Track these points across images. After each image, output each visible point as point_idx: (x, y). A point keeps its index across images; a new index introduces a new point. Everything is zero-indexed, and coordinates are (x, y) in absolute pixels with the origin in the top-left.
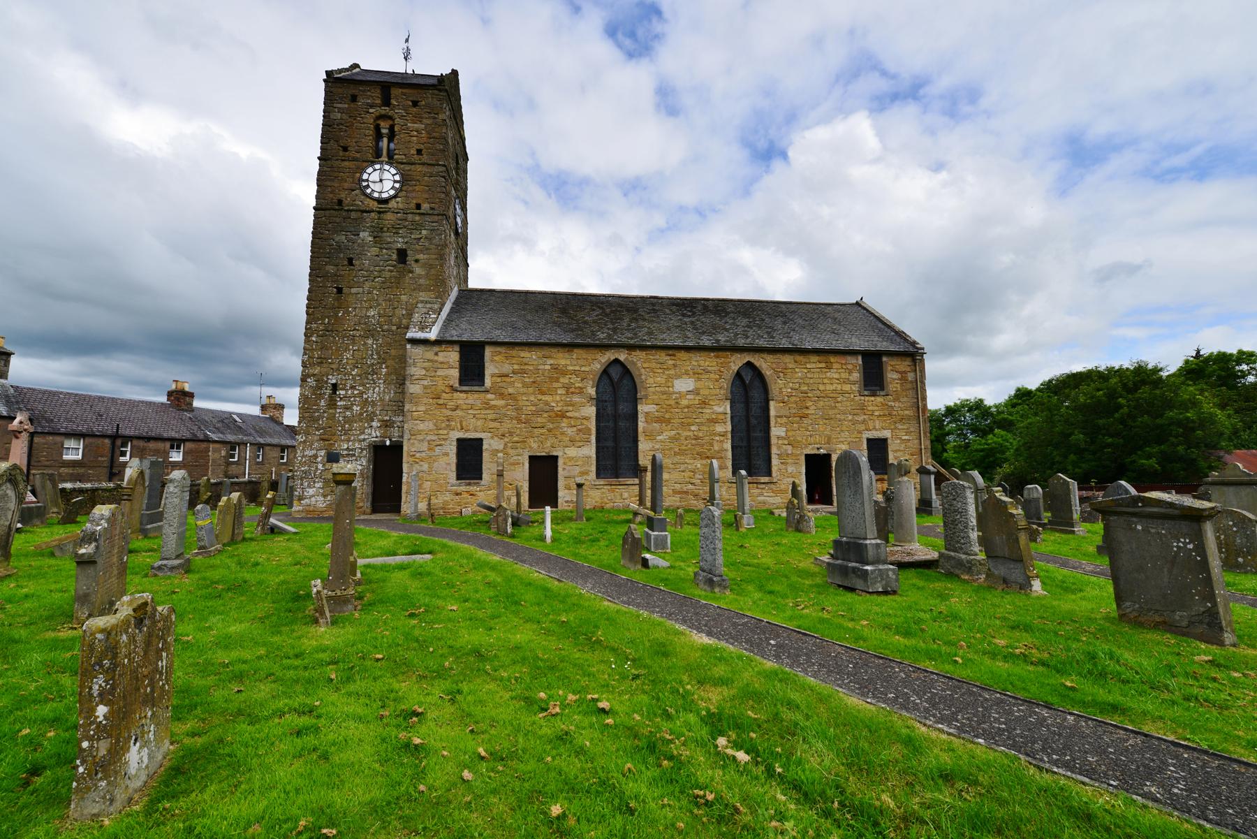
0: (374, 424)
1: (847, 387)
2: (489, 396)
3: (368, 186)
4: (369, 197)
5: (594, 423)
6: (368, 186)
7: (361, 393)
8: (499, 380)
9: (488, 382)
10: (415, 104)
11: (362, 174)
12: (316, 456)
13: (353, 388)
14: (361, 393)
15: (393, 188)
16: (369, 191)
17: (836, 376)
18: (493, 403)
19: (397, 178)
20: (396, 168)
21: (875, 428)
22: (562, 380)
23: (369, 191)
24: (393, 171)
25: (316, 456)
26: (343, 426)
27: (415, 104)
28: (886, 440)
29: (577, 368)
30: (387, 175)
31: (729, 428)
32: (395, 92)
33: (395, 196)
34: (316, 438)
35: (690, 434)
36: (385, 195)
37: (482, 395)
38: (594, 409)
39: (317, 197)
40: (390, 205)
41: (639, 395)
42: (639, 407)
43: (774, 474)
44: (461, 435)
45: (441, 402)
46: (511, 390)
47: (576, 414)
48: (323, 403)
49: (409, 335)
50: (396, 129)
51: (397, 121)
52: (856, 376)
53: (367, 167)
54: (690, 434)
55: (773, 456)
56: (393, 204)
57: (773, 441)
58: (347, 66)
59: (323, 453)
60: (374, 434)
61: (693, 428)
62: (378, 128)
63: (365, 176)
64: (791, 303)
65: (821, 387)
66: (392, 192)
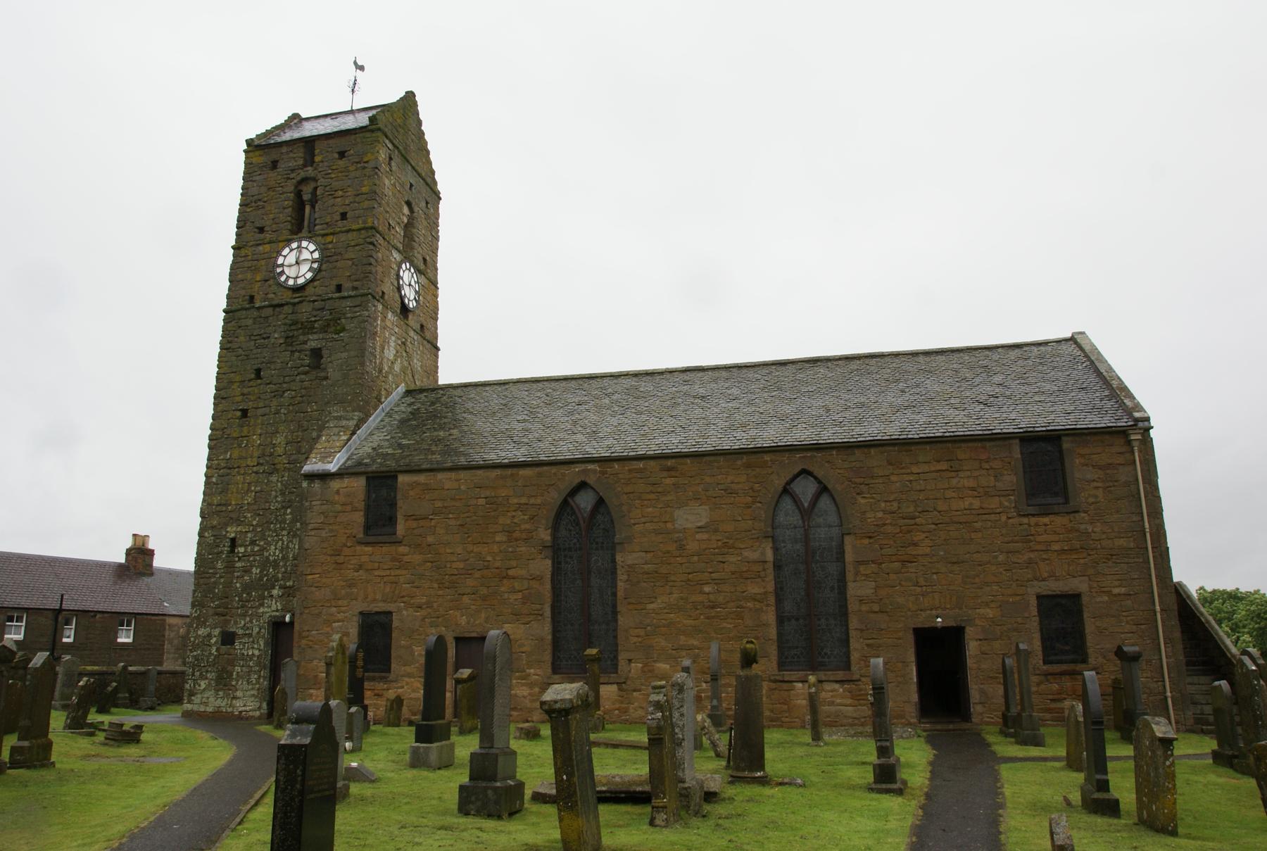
0: (275, 592)
1: (993, 503)
2: (402, 549)
3: (283, 272)
4: (283, 286)
5: (548, 586)
6: (283, 272)
7: (263, 549)
8: (414, 524)
9: (401, 528)
10: (342, 155)
11: (276, 258)
12: (209, 636)
13: (253, 543)
14: (263, 549)
15: (311, 269)
16: (291, 282)
17: (971, 483)
18: (406, 559)
19: (316, 255)
20: (316, 243)
21: (1052, 575)
22: (501, 521)
23: (283, 279)
24: (312, 247)
25: (209, 636)
26: (240, 596)
27: (342, 155)
28: (1077, 596)
29: (524, 500)
30: (306, 255)
31: (771, 587)
32: (319, 147)
33: (312, 280)
34: (211, 612)
35: (700, 598)
36: (301, 281)
37: (393, 548)
38: (549, 562)
39: (228, 297)
40: (306, 293)
41: (617, 538)
42: (619, 558)
43: (854, 668)
44: (365, 607)
45: (341, 559)
46: (430, 539)
47: (522, 572)
48: (219, 565)
49: (307, 468)
50: (318, 192)
51: (322, 181)
52: (1011, 479)
53: (283, 248)
54: (700, 598)
55: (852, 633)
56: (310, 290)
57: (853, 606)
58: (281, 120)
59: (217, 632)
60: (272, 608)
61: (707, 589)
62: (299, 194)
63: (280, 261)
64: (1045, 343)
65: (941, 506)
66: (309, 275)
